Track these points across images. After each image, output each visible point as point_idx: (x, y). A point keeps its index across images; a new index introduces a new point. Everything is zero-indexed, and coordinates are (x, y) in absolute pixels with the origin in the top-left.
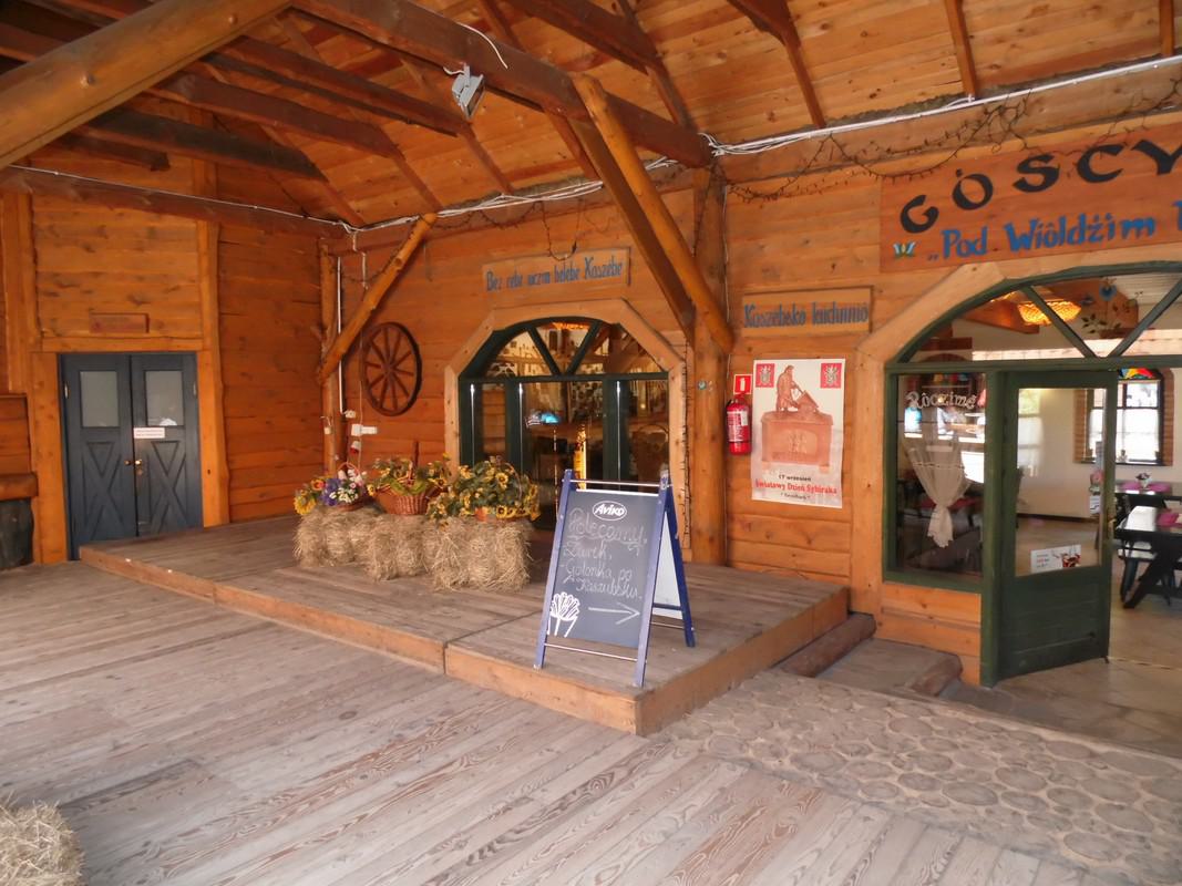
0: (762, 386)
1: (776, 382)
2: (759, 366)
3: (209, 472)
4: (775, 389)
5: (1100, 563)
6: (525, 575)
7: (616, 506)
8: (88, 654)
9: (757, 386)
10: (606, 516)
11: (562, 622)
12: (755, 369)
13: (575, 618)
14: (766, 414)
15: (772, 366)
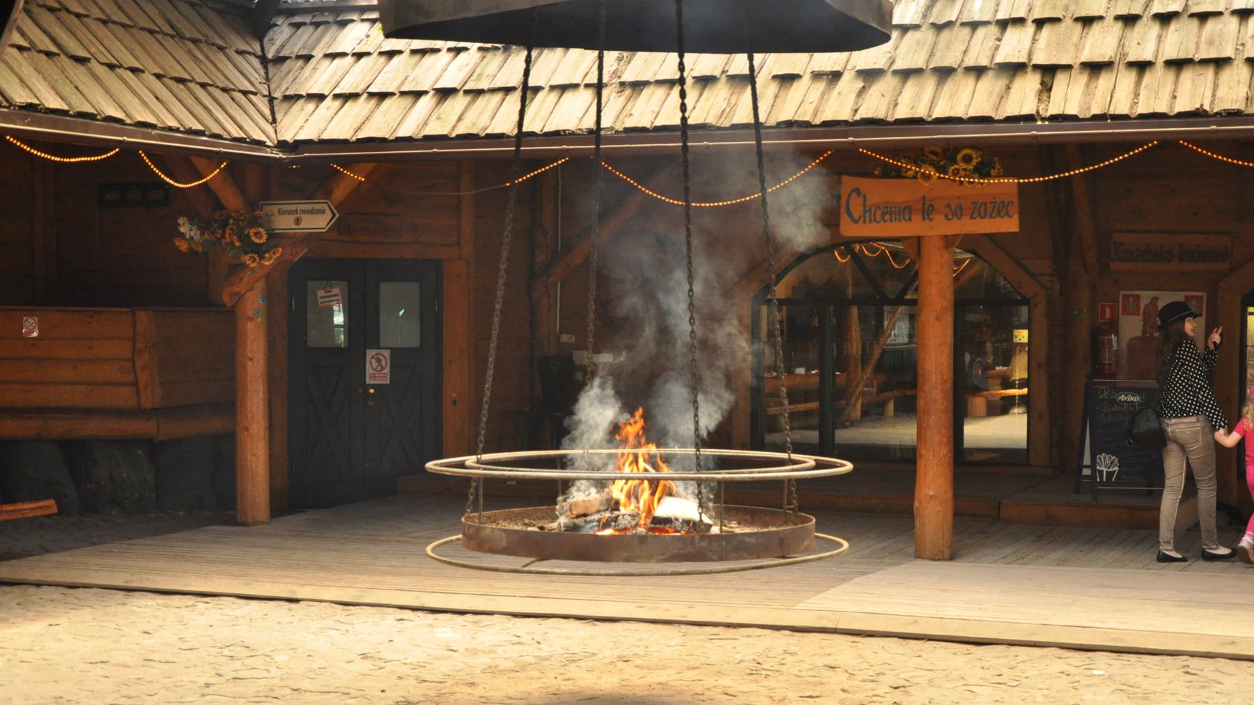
0: (1128, 314)
1: (1141, 311)
2: (1125, 297)
3: (1041, 417)
4: (1141, 317)
5: (970, 398)
6: (199, 232)
7: (1132, 395)
8: (916, 326)
9: (1123, 314)
10: (1126, 402)
11: (1107, 472)
12: (1121, 299)
13: (1116, 468)
14: (1131, 339)
15: (1138, 298)
